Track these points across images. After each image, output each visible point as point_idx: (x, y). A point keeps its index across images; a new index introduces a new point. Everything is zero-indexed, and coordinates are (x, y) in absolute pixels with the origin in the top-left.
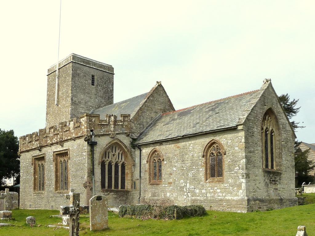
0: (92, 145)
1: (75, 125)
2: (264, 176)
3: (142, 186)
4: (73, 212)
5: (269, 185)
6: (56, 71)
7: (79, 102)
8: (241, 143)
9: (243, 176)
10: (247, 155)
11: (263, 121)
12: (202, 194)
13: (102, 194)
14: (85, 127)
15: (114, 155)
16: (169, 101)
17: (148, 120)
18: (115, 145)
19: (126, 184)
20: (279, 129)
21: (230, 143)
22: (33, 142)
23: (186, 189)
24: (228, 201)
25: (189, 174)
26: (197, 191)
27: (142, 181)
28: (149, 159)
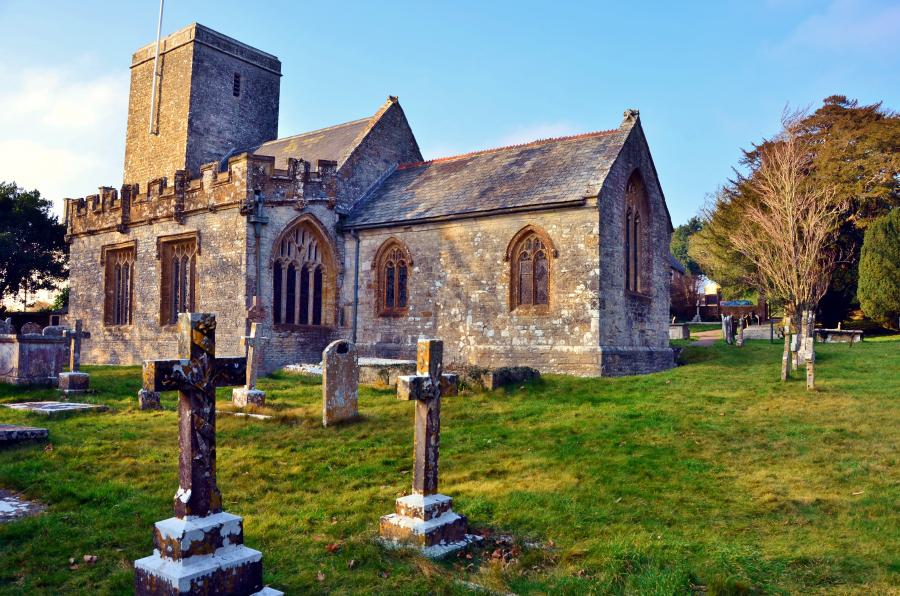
0: (257, 224)
1: (216, 177)
2: (627, 305)
4: (429, 392)
8: (592, 236)
9: (594, 304)
12: (503, 340)
14: (242, 184)
15: (300, 249)
16: (413, 139)
17: (372, 177)
18: (302, 227)
19: (323, 314)
20: (648, 212)
22: (106, 215)
23: (465, 328)
24: (561, 355)
27: (359, 307)
28: (377, 259)
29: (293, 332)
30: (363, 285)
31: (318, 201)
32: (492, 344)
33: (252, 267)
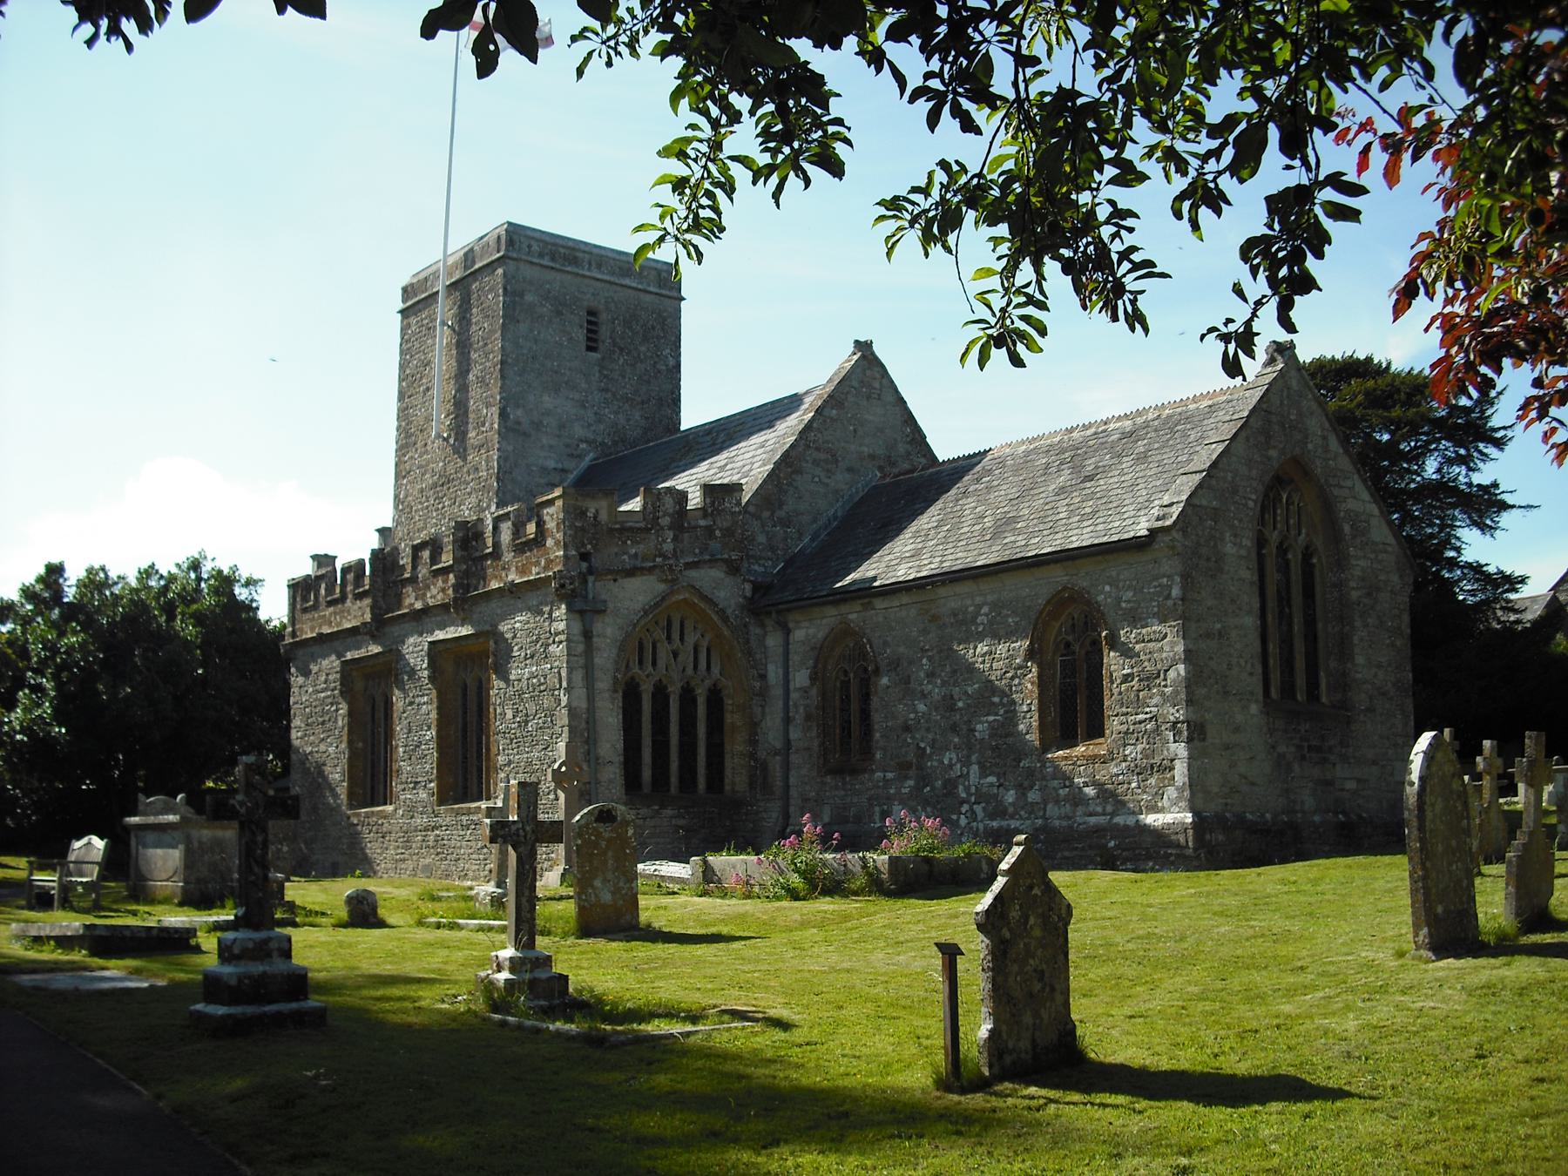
0: (585, 609)
3: (792, 780)
5: (1296, 767)
6: (437, 292)
7: (532, 422)
8: (1170, 603)
10: (1190, 646)
11: (1263, 509)
12: (1032, 809)
13: (621, 809)
14: (557, 543)
15: (675, 654)
16: (910, 419)
21: (1128, 602)
23: (967, 789)
25: (979, 727)
26: (1010, 797)
29: (663, 807)
30: (799, 716)
31: (705, 562)
32: (1012, 817)
33: (581, 692)
